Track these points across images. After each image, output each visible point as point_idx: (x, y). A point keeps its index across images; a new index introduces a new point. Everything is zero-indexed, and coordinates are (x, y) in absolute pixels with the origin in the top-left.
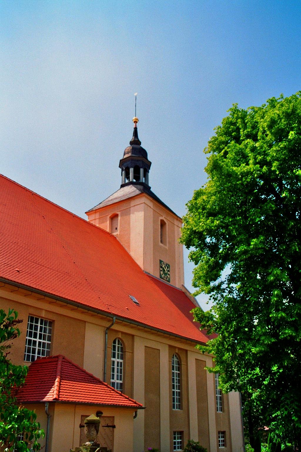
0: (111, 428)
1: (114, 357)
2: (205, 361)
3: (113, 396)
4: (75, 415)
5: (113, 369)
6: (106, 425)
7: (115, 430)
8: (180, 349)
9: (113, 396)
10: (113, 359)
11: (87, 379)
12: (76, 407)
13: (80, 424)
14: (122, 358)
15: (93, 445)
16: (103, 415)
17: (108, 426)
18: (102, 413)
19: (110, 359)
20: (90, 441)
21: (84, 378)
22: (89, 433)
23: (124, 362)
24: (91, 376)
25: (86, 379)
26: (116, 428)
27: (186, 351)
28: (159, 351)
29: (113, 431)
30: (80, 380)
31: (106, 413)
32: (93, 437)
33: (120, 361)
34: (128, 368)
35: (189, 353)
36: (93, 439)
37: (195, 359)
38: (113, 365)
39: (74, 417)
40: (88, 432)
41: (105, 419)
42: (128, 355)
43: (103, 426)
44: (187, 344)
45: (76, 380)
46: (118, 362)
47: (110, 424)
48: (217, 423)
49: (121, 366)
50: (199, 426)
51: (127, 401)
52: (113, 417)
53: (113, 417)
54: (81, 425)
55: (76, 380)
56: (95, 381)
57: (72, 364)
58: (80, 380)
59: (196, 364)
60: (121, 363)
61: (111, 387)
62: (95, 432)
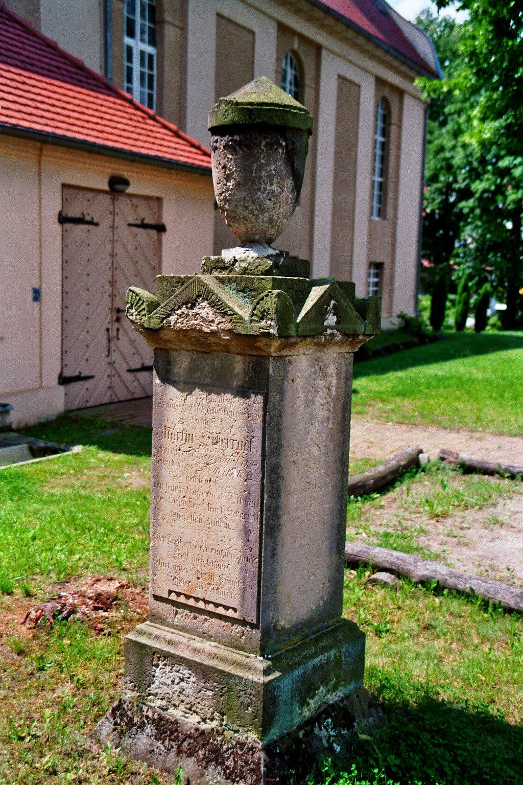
0: (153, 233)
1: (131, 34)
2: (359, 86)
3: (155, 135)
4: (40, 184)
5: (130, 71)
6: (139, 222)
7: (165, 237)
8: (304, 39)
9: (155, 135)
10: (128, 41)
11: (68, 71)
12: (45, 152)
13: (60, 214)
14: (153, 42)
15: (276, 264)
16: (130, 190)
17: (143, 226)
18: (127, 183)
19: (121, 40)
20: (248, 242)
21: (57, 67)
22: (252, 191)
23: (161, 56)
24: (79, 66)
25: (65, 73)
26: (168, 233)
27: (318, 48)
28: (251, 36)
29: (160, 241)
30: (43, 68)
31: (140, 184)
32: (270, 221)
33: (150, 49)
34: (171, 76)
35: (325, 55)
36: (271, 232)
37: (336, 77)
38: (130, 59)
39: (36, 191)
40: (238, 185)
41: (135, 201)
42: (170, 34)
43: (130, 225)
44: (322, 26)
45: (29, 67)
46: (142, 53)
47: (149, 220)
48: (371, 247)
49: (151, 67)
50: (333, 248)
51: (197, 154)
52: (159, 199)
53: (159, 199)
54: (64, 214)
55: (29, 67)
56: (94, 82)
57: (8, 14)
58: (43, 68)
59: (340, 89)
60: (151, 57)
61: (146, 108)
62: (287, 195)
